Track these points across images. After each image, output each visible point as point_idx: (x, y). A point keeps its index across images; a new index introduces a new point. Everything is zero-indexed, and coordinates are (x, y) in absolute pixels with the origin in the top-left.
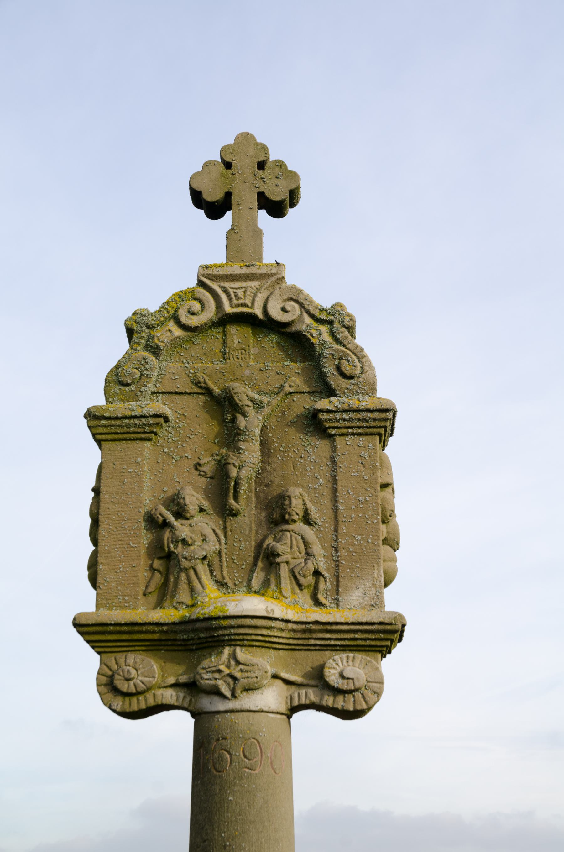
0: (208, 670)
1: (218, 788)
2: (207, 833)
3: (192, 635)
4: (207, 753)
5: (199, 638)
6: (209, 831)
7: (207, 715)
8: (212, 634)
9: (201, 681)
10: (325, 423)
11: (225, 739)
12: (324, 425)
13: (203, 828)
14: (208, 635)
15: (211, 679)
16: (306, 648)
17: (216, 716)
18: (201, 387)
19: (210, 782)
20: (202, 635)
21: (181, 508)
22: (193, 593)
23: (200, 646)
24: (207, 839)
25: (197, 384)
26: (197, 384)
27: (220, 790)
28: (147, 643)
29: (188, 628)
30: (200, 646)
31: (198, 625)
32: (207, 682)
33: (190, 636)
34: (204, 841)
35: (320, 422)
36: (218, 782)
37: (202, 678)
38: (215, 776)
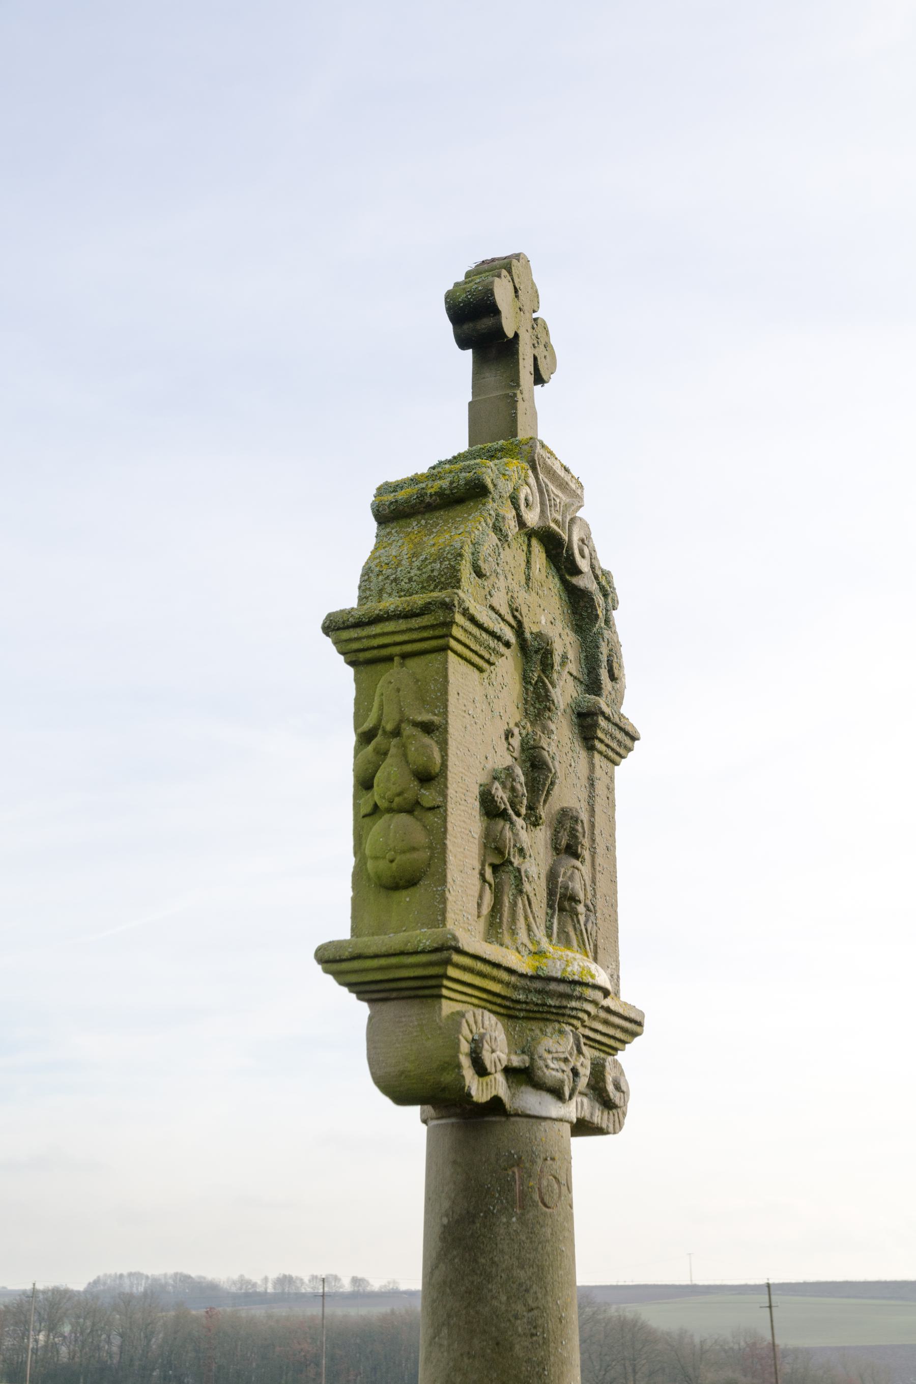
0: (555, 1055)
1: (549, 1231)
2: (537, 1298)
3: (535, 998)
4: (530, 1176)
5: (544, 1005)
6: (540, 1296)
7: (534, 1120)
8: (565, 1003)
9: (545, 1070)
10: (598, 731)
11: (553, 1159)
12: (596, 733)
13: (527, 1291)
14: (557, 1004)
15: (557, 1070)
16: (591, 1044)
17: (543, 1124)
18: (515, 617)
19: (538, 1222)
20: (550, 1002)
21: (516, 797)
22: (531, 933)
23: (531, 1015)
24: (538, 1308)
25: (514, 610)
26: (514, 610)
27: (552, 1234)
28: (484, 996)
29: (535, 986)
30: (531, 1015)
31: (553, 986)
32: (554, 1073)
33: (530, 997)
34: (531, 1310)
35: (596, 725)
36: (550, 1223)
37: (547, 1066)
38: (545, 1214)
